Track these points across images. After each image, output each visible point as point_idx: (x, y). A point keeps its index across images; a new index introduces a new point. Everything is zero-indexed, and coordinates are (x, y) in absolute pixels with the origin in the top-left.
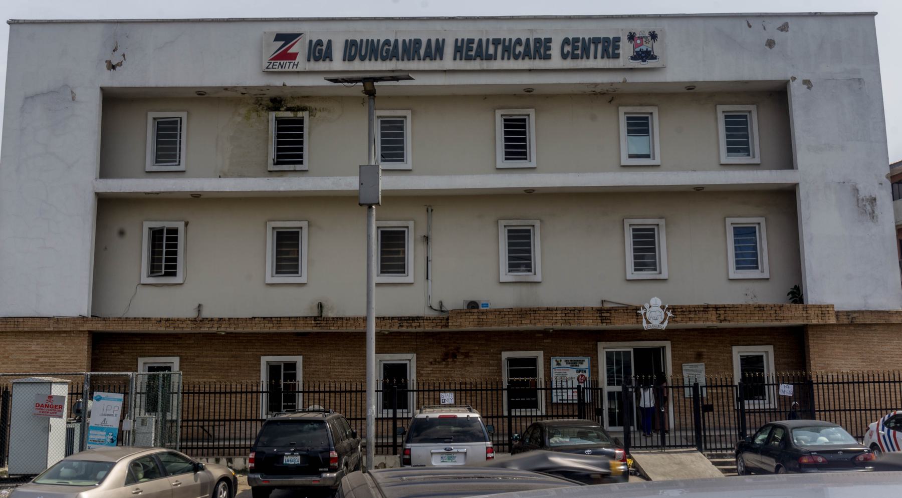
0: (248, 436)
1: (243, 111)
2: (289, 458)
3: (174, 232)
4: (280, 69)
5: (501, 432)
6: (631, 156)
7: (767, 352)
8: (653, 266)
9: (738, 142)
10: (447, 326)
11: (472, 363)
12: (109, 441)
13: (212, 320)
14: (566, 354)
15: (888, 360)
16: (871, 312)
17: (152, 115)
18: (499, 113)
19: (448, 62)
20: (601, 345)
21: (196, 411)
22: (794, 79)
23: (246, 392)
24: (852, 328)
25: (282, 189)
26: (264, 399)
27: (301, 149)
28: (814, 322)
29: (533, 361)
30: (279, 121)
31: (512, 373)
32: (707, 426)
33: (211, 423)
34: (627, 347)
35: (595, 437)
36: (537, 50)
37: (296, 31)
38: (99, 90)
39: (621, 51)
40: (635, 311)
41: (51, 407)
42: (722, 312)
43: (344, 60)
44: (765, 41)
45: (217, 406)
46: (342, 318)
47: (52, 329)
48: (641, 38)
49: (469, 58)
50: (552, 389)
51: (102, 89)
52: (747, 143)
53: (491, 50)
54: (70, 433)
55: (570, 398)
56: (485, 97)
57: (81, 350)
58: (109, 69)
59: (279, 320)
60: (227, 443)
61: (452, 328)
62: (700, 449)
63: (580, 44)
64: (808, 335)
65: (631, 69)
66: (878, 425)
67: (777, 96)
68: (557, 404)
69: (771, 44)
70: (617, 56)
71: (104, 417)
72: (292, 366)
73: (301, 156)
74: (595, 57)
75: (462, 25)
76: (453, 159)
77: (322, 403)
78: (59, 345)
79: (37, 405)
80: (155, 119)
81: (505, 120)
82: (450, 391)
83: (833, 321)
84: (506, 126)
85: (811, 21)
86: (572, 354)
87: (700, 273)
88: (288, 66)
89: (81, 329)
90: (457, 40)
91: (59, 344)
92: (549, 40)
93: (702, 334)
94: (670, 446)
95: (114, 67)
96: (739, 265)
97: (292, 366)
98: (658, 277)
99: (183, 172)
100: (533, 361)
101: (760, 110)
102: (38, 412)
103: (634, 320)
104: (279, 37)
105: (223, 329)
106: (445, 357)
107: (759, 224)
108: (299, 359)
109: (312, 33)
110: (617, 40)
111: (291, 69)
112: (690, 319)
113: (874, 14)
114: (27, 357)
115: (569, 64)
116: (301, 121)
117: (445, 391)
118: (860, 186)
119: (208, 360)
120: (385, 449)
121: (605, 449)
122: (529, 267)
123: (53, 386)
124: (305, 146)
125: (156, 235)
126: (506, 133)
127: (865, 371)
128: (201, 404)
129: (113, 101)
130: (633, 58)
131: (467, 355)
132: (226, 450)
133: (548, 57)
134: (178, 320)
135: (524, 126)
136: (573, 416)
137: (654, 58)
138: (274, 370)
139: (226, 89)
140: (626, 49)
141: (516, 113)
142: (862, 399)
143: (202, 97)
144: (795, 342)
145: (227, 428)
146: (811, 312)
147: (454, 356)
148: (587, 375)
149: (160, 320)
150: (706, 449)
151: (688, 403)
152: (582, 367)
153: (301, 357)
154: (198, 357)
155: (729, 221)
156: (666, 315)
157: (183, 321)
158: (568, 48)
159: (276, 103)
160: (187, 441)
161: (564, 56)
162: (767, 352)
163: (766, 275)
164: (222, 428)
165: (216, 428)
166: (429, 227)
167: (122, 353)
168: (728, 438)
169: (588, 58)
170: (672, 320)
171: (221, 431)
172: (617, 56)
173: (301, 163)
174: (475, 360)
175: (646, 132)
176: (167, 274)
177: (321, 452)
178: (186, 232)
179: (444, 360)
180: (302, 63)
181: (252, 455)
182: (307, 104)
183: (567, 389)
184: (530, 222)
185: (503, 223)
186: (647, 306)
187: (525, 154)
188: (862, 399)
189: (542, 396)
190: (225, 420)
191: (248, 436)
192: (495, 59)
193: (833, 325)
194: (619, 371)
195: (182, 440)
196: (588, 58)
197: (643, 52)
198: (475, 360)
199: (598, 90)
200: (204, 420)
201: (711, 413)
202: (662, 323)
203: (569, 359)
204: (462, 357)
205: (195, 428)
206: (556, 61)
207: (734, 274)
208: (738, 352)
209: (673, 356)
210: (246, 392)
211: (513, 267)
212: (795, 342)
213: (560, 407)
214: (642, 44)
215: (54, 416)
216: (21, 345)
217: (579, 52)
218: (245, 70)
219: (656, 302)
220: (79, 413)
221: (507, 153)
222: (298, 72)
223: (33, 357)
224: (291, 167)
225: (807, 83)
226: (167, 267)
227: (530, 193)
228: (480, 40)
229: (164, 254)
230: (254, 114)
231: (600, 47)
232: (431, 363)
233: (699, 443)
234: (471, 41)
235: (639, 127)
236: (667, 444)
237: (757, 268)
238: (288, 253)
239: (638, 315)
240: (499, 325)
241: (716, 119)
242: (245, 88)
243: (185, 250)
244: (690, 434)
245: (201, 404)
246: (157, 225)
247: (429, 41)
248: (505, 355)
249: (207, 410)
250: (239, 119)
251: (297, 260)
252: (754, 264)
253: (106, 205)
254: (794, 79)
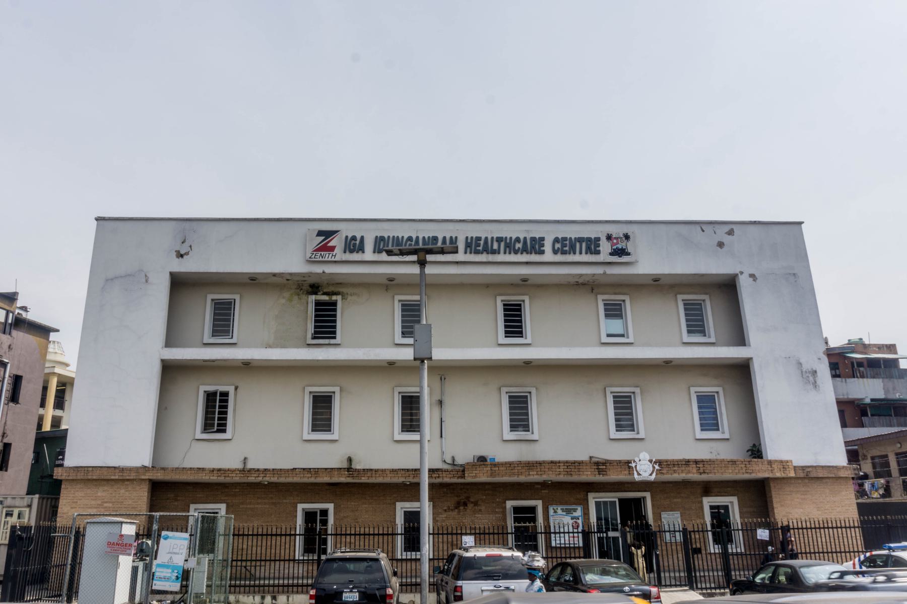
0: (286, 576)
1: (287, 294)
2: (348, 594)
3: (225, 395)
4: (321, 259)
5: (677, 568)
6: (609, 335)
7: (732, 503)
8: (632, 427)
9: (696, 325)
10: (463, 477)
11: (480, 510)
12: (174, 578)
13: (258, 470)
14: (561, 504)
15: (838, 509)
16: (823, 467)
17: (210, 297)
18: (499, 299)
19: (461, 256)
20: (591, 496)
21: (240, 553)
22: (742, 273)
23: (286, 535)
24: (807, 481)
25: (320, 358)
26: (299, 542)
27: (335, 327)
28: (778, 475)
29: (533, 510)
30: (318, 303)
31: (516, 520)
32: (697, 567)
33: (253, 563)
34: (612, 497)
35: (623, 575)
36: (533, 247)
37: (334, 229)
38: (168, 277)
39: (601, 248)
40: (627, 465)
41: (118, 546)
42: (701, 466)
43: (374, 252)
45: (259, 549)
46: (371, 470)
47: (117, 477)
48: (617, 238)
49: (477, 252)
50: (550, 533)
51: (171, 274)
52: (703, 326)
53: (495, 246)
54: (135, 570)
55: (567, 542)
56: (488, 286)
57: (141, 497)
58: (178, 257)
59: (317, 471)
60: (262, 582)
61: (469, 479)
62: (692, 588)
63: (567, 242)
64: (770, 487)
65: (610, 263)
66: (854, 564)
67: (728, 288)
68: (556, 547)
70: (598, 253)
71: (170, 555)
72: (324, 513)
73: (335, 333)
74: (581, 253)
75: (470, 226)
76: (466, 336)
77: (348, 545)
78: (122, 492)
79: (109, 544)
80: (212, 300)
81: (504, 305)
82: (470, 534)
83: (792, 474)
84: (505, 310)
85: (752, 227)
86: (566, 503)
87: (668, 436)
88: (328, 256)
89: (143, 477)
90: (467, 238)
91: (123, 491)
92: (542, 239)
93: (682, 485)
94: (666, 586)
95: (182, 256)
96: (704, 427)
97: (324, 513)
98: (637, 436)
99: (235, 344)
100: (533, 510)
101: (716, 298)
102: (109, 550)
103: (627, 472)
104: (320, 233)
105: (267, 479)
106: (458, 506)
107: (717, 392)
108: (330, 507)
109: (348, 231)
110: (598, 239)
111: (330, 259)
113: (801, 223)
114: (93, 502)
115: (559, 258)
116: (334, 304)
117: (466, 534)
118: (802, 361)
119: (252, 506)
120: (409, 587)
122: (526, 428)
123: (124, 525)
124: (339, 324)
125: (210, 397)
126: (505, 315)
127: (821, 519)
128: (245, 547)
129: (181, 285)
130: (611, 254)
131: (476, 504)
132: (271, 588)
133: (542, 252)
134: (229, 470)
135: (520, 310)
136: (580, 557)
137: (628, 254)
138: (310, 516)
139: (274, 275)
140: (605, 247)
141: (514, 299)
142: (820, 543)
143: (254, 283)
144: (758, 494)
145: (267, 567)
146: (775, 466)
147: (465, 504)
148: (580, 522)
149: (213, 470)
150: (697, 588)
151: (679, 548)
152: (575, 514)
153: (332, 505)
154: (242, 503)
155: (693, 390)
156: (654, 467)
157: (233, 471)
158: (558, 246)
159: (314, 288)
160: (236, 579)
161: (555, 252)
162: (732, 502)
163: (727, 436)
164: (263, 568)
165: (258, 568)
166: (442, 393)
167: (176, 500)
168: (707, 578)
169: (575, 253)
170: (659, 472)
171: (263, 571)
172: (598, 253)
173: (335, 338)
174: (483, 508)
175: (620, 316)
176: (218, 431)
177: (378, 589)
178: (236, 395)
179: (456, 508)
180: (339, 254)
181: (313, 592)
182: (341, 290)
183: (564, 533)
184: (528, 389)
185: (504, 390)
186: (637, 459)
187: (521, 332)
188: (820, 543)
189: (541, 539)
190: (266, 560)
191: (286, 576)
192: (499, 253)
193: (791, 478)
195: (231, 579)
196: (575, 253)
197: (619, 250)
198: (483, 508)
199: (581, 281)
200: (246, 561)
201: (700, 556)
202: (651, 475)
203: (565, 507)
204: (472, 505)
205: (239, 568)
206: (549, 256)
207: (700, 435)
208: (708, 502)
209: (653, 506)
210: (286, 535)
211: (513, 428)
212: (758, 494)
213: (558, 550)
214: (617, 243)
215: (124, 554)
216: (89, 491)
217: (567, 248)
218: (292, 260)
219: (645, 456)
220: (145, 554)
221: (506, 332)
222: (335, 262)
223: (99, 502)
224: (326, 341)
225: (752, 276)
226: (219, 425)
227: (528, 365)
228: (486, 238)
229: (216, 412)
230: (296, 297)
231: (584, 245)
232: (445, 511)
233: (691, 583)
234: (479, 239)
235: (614, 311)
236: (663, 583)
237: (718, 430)
238: (322, 414)
239: (630, 467)
240: (510, 476)
241: (677, 307)
242: (291, 274)
243: (234, 410)
244: (682, 574)
245: (245, 547)
246: (211, 388)
247: (444, 238)
248: (510, 504)
249: (249, 552)
250: (283, 301)
251: (330, 420)
252: (715, 427)
253: (171, 371)
254: (742, 273)
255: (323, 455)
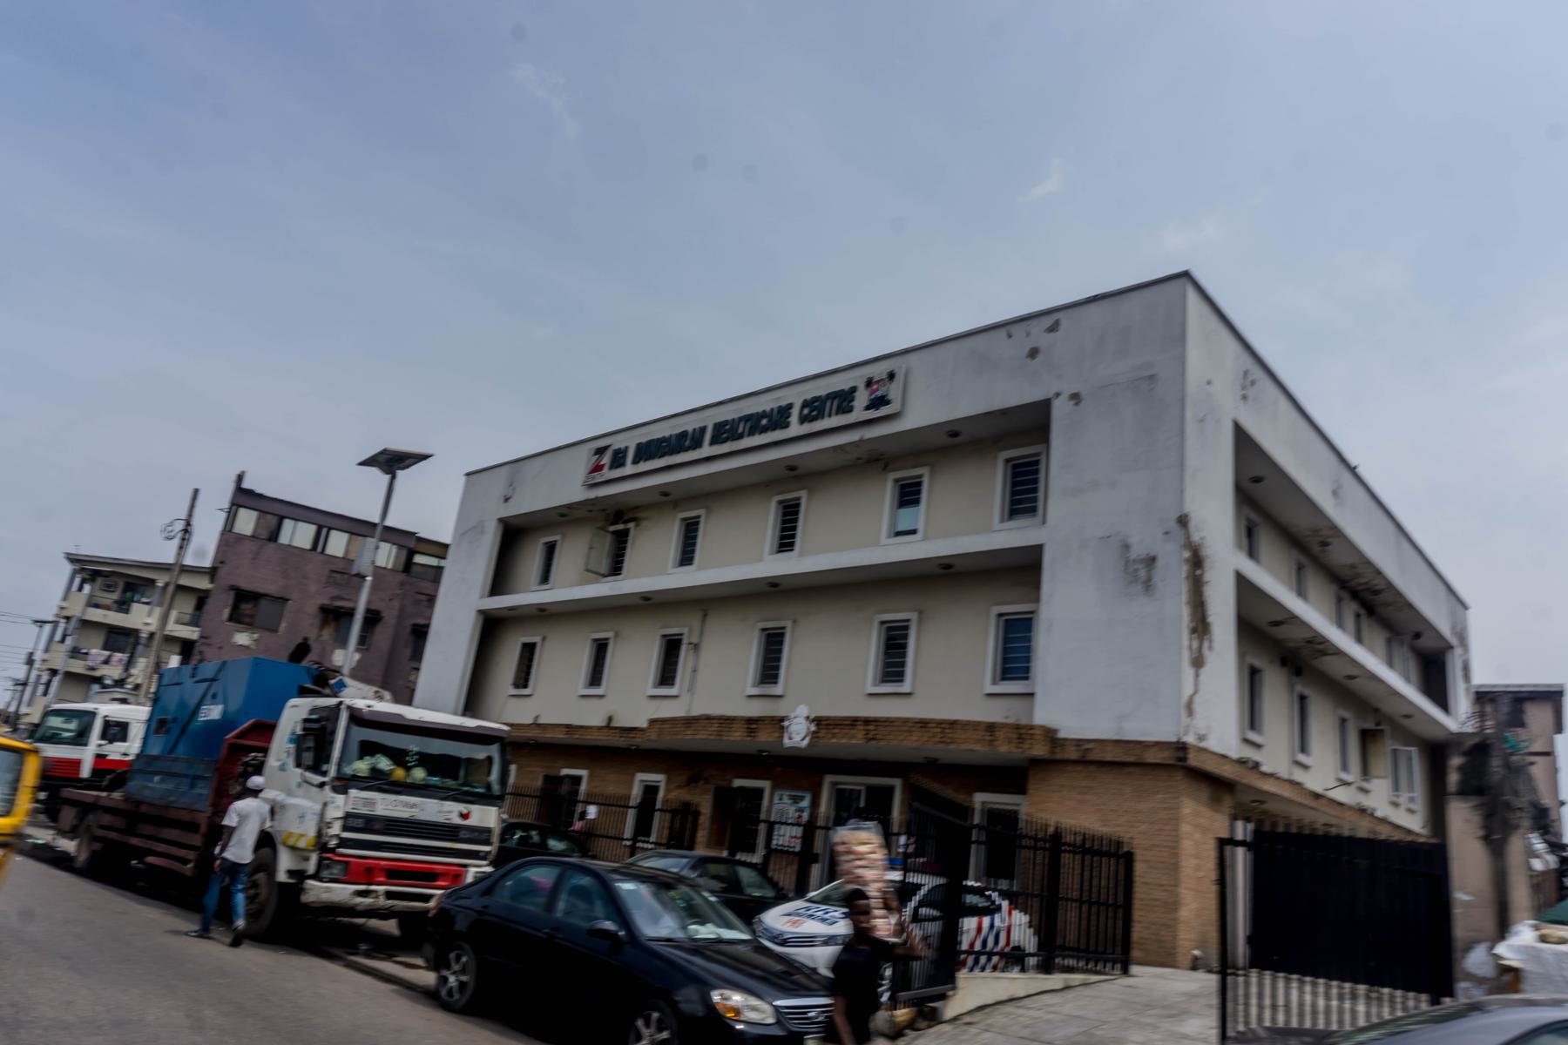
20: (828, 779)
22: (1058, 395)
44: (1026, 351)
69: (1033, 353)
85: (1092, 307)
108: (583, 773)
112: (834, 735)
118: (1133, 540)
121: (706, 894)
130: (868, 408)
140: (862, 398)
166: (701, 634)
194: (398, 756)
255: (590, 715)
